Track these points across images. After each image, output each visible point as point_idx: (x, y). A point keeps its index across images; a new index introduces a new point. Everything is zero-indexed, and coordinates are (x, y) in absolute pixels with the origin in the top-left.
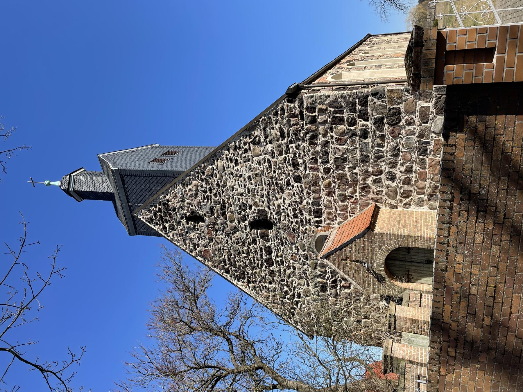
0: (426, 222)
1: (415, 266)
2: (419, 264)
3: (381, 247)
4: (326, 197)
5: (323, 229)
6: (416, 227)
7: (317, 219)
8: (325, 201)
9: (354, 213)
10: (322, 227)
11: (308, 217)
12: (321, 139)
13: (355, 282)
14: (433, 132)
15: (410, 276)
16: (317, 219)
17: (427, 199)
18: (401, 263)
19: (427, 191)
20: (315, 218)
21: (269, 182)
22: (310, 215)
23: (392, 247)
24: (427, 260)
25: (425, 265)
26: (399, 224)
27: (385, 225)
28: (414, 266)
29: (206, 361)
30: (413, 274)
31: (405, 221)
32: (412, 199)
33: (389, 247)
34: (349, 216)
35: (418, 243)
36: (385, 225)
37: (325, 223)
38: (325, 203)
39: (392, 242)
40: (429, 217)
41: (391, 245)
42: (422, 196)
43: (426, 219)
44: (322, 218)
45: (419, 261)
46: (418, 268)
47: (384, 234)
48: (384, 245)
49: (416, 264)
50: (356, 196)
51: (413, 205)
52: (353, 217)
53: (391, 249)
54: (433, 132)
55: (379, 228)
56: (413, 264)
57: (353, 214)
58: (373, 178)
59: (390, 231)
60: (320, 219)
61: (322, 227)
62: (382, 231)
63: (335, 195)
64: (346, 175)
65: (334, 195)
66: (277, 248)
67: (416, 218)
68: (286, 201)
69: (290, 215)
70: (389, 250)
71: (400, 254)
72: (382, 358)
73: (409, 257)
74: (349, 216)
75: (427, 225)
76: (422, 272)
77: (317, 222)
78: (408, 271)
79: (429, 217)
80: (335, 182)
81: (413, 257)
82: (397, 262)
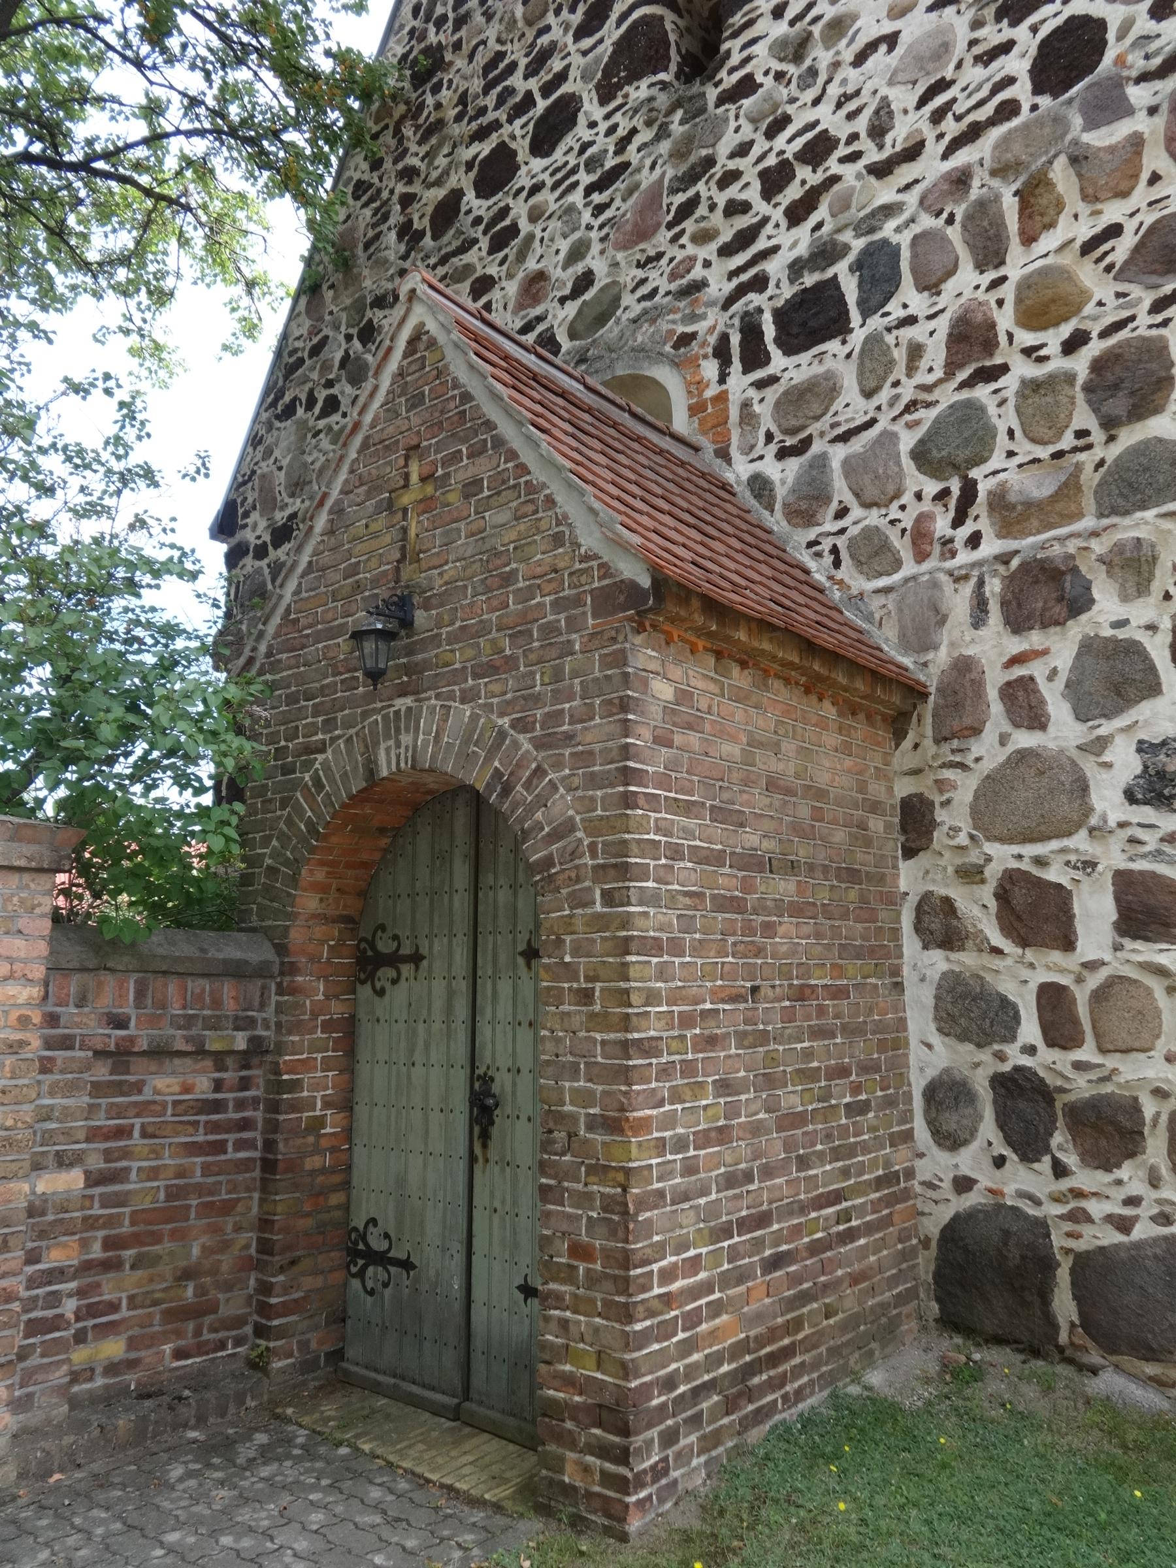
0: (808, 1075)
1: (449, 1010)
2: (462, 1036)
3: (522, 725)
4: (943, 325)
5: (709, 393)
6: (735, 999)
8: (907, 333)
9: (837, 564)
10: (722, 380)
11: (775, 267)
13: (297, 592)
15: (392, 973)
17: (1006, 1067)
18: (460, 903)
19: (1078, 1066)
21: (950, 1121)
22: (796, 268)
23: (530, 810)
24: (496, 1088)
25: (460, 1078)
26: (751, 862)
27: (731, 750)
28: (451, 995)
30: (399, 995)
31: (796, 910)
32: (997, 951)
33: (528, 786)
34: (812, 534)
35: (576, 1021)
36: (731, 750)
37: (752, 393)
38: (890, 339)
39: (564, 804)
40: (856, 1089)
41: (542, 802)
42: (1030, 1030)
43: (844, 1072)
44: (778, 361)
45: (485, 1032)
46: (437, 1026)
47: (626, 728)
48: (539, 744)
49: (462, 1010)
50: (974, 540)
51: (944, 966)
52: (812, 565)
53: (515, 806)
55: (684, 696)
56: (463, 986)
57: (828, 559)
58: (1152, 628)
59: (663, 781)
60: (772, 348)
61: (722, 380)
62: (655, 711)
63: (963, 385)
65: (963, 375)
66: (574, 171)
67: (839, 993)
68: (879, 60)
69: (780, 141)
70: (507, 790)
73: (503, 958)
74: (812, 534)
75: (770, 1082)
77: (751, 330)
79: (856, 1089)
80: (1072, 346)
81: (505, 988)
82: (461, 872)
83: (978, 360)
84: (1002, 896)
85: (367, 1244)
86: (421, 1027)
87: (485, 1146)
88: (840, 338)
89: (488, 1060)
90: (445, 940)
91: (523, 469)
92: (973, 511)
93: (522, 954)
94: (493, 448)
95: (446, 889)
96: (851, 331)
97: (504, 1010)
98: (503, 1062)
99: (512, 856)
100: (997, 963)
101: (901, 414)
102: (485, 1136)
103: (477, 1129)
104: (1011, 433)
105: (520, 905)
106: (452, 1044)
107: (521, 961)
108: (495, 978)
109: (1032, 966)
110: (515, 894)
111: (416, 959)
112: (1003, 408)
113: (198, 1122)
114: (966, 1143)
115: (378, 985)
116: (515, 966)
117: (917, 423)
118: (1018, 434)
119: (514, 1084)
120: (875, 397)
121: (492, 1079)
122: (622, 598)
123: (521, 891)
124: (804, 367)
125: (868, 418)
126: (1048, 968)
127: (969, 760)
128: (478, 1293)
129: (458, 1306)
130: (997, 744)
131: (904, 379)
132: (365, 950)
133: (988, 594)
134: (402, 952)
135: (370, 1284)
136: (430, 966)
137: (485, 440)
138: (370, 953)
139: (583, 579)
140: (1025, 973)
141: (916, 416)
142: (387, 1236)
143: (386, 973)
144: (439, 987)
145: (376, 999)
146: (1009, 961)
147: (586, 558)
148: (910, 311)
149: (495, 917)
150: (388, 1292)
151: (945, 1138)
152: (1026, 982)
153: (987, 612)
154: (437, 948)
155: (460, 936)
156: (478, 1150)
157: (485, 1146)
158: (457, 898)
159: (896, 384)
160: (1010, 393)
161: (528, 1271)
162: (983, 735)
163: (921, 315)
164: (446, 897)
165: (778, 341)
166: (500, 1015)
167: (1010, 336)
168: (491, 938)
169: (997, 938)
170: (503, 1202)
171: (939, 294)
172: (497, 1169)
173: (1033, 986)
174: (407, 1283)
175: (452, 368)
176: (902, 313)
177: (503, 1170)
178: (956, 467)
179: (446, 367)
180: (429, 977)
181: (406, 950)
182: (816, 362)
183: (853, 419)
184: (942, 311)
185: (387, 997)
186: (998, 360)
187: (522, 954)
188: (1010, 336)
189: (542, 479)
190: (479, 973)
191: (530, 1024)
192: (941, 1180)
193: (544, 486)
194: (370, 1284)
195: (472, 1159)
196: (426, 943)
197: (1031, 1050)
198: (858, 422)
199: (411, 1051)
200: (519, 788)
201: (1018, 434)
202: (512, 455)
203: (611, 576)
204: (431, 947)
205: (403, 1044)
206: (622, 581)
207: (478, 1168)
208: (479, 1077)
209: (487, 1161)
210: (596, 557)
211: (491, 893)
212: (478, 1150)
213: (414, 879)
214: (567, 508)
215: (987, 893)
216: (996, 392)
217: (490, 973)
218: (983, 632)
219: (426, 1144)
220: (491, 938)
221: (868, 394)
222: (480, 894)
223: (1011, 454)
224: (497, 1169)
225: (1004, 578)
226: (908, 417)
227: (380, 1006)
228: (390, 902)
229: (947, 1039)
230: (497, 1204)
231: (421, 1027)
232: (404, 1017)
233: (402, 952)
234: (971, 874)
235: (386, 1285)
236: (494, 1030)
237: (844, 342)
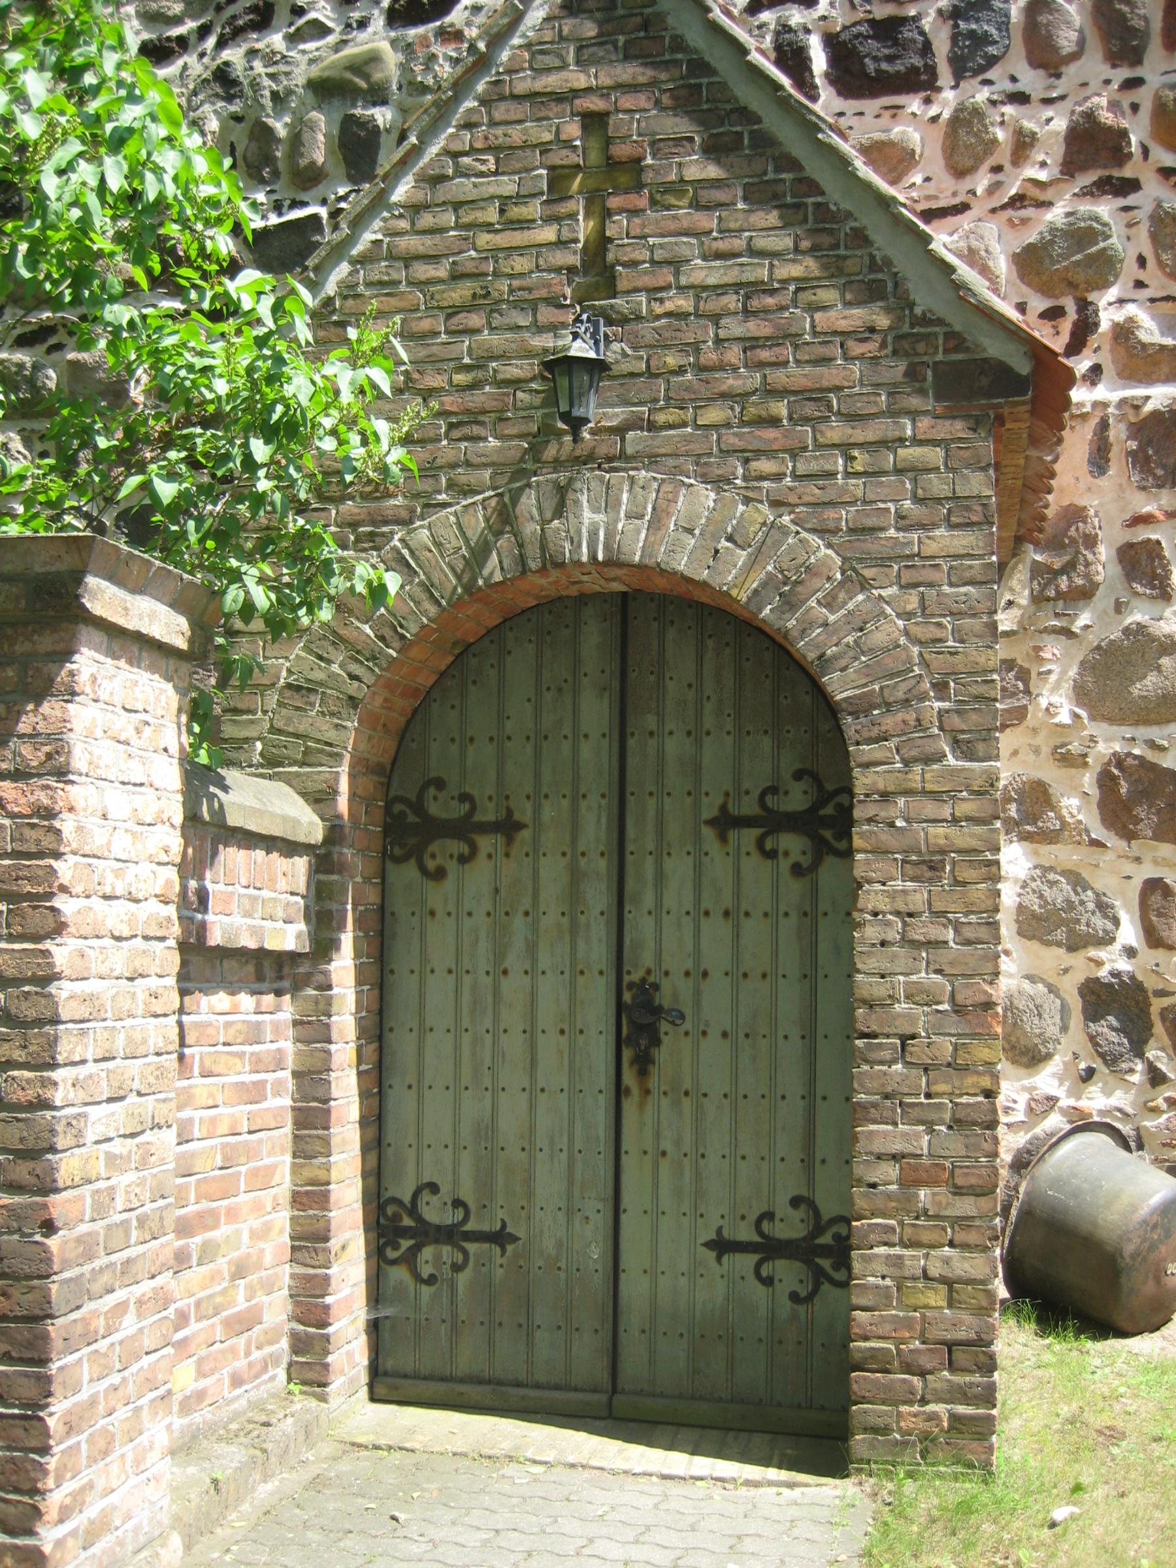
7: (819, 61)
12: (33, 524)
14: (813, 321)
15: (458, 847)
16: (819, 61)
20: (831, 42)
24: (664, 998)
28: (576, 877)
29: (702, 303)
30: (480, 874)
45: (640, 925)
46: (551, 918)
49: (598, 897)
54: (813, 321)
64: (1070, 167)
70: (790, 603)
71: (695, 734)
72: (768, 212)
73: (673, 829)
76: (515, 960)
78: (508, 827)
81: (679, 867)
83: (1105, 167)
84: (1106, 781)
85: (419, 1219)
86: (519, 923)
87: (643, 1073)
88: (923, 94)
89: (648, 960)
90: (565, 803)
91: (815, 188)
92: (1093, 341)
93: (711, 822)
94: (752, 147)
95: (567, 730)
96: (939, 90)
97: (679, 894)
98: (676, 960)
99: (691, 695)
100: (1095, 855)
101: (1004, 207)
102: (644, 1063)
103: (627, 1054)
104: (1142, 261)
105: (707, 759)
106: (581, 945)
107: (708, 833)
108: (660, 853)
109: (1138, 860)
110: (699, 744)
111: (508, 827)
112: (1134, 230)
113: (244, 1053)
114: (1048, 1056)
115: (431, 865)
116: (698, 838)
117: (1024, 221)
118: (1151, 262)
119: (697, 993)
120: (968, 178)
121: (656, 987)
122: (985, 381)
123: (707, 741)
124: (869, 118)
125: (957, 201)
126: (1155, 862)
127: (1076, 628)
128: (628, 1259)
129: (598, 1281)
130: (1111, 612)
131: (1008, 166)
132: (402, 813)
133: (1112, 439)
134: (478, 817)
135: (426, 1271)
136: (535, 841)
137: (740, 135)
138: (412, 818)
139: (921, 347)
140: (1129, 868)
141: (1023, 213)
142: (458, 1203)
143: (444, 850)
144: (553, 870)
145: (430, 885)
146: (1109, 856)
147: (924, 320)
148: (1020, 87)
149: (660, 772)
150: (463, 1278)
151: (1022, 1054)
152: (1129, 877)
153: (1108, 460)
154: (548, 813)
155: (594, 799)
156: (629, 1078)
157: (643, 1073)
158: (586, 750)
159: (997, 169)
160: (1142, 215)
161: (721, 1222)
162: (1095, 599)
163: (1036, 95)
164: (566, 746)
165: (830, 78)
166: (670, 901)
167: (1145, 151)
168: (651, 803)
169: (1098, 832)
170: (678, 1143)
171: (1058, 76)
172: (665, 1102)
173: (1137, 883)
174: (499, 1261)
175: (670, 21)
176: (1009, 87)
177: (676, 1103)
178: (1072, 285)
179: (660, 17)
180: (535, 851)
181: (488, 813)
182: (887, 114)
183: (936, 198)
184: (1062, 98)
185: (449, 884)
186: (1128, 172)
187: (711, 822)
188: (1145, 151)
189: (846, 205)
190: (630, 847)
191: (727, 914)
192: (1015, 1102)
193: (849, 215)
194: (426, 1271)
195: (619, 1091)
196: (528, 806)
197: (1130, 952)
198: (942, 203)
199: (499, 954)
200: (812, 603)
201: (1151, 262)
202: (794, 165)
203: (967, 350)
204: (537, 810)
205: (484, 945)
206: (985, 360)
207: (630, 1106)
208: (631, 986)
209: (647, 1092)
210: (940, 322)
211: (652, 743)
212: (629, 1078)
213: (502, 717)
214: (890, 252)
215: (1088, 780)
216: (1126, 209)
217: (650, 846)
218: (1103, 482)
219: (532, 1077)
220: (651, 803)
221: (960, 173)
222: (631, 742)
223: (1139, 284)
224: (665, 1102)
225: (1131, 425)
226: (1010, 213)
227: (437, 895)
228: (454, 748)
229: (1029, 943)
230: (666, 1145)
231: (519, 923)
232: (487, 905)
233: (478, 817)
234: (1069, 760)
235: (457, 1268)
236: (659, 923)
237: (928, 101)
